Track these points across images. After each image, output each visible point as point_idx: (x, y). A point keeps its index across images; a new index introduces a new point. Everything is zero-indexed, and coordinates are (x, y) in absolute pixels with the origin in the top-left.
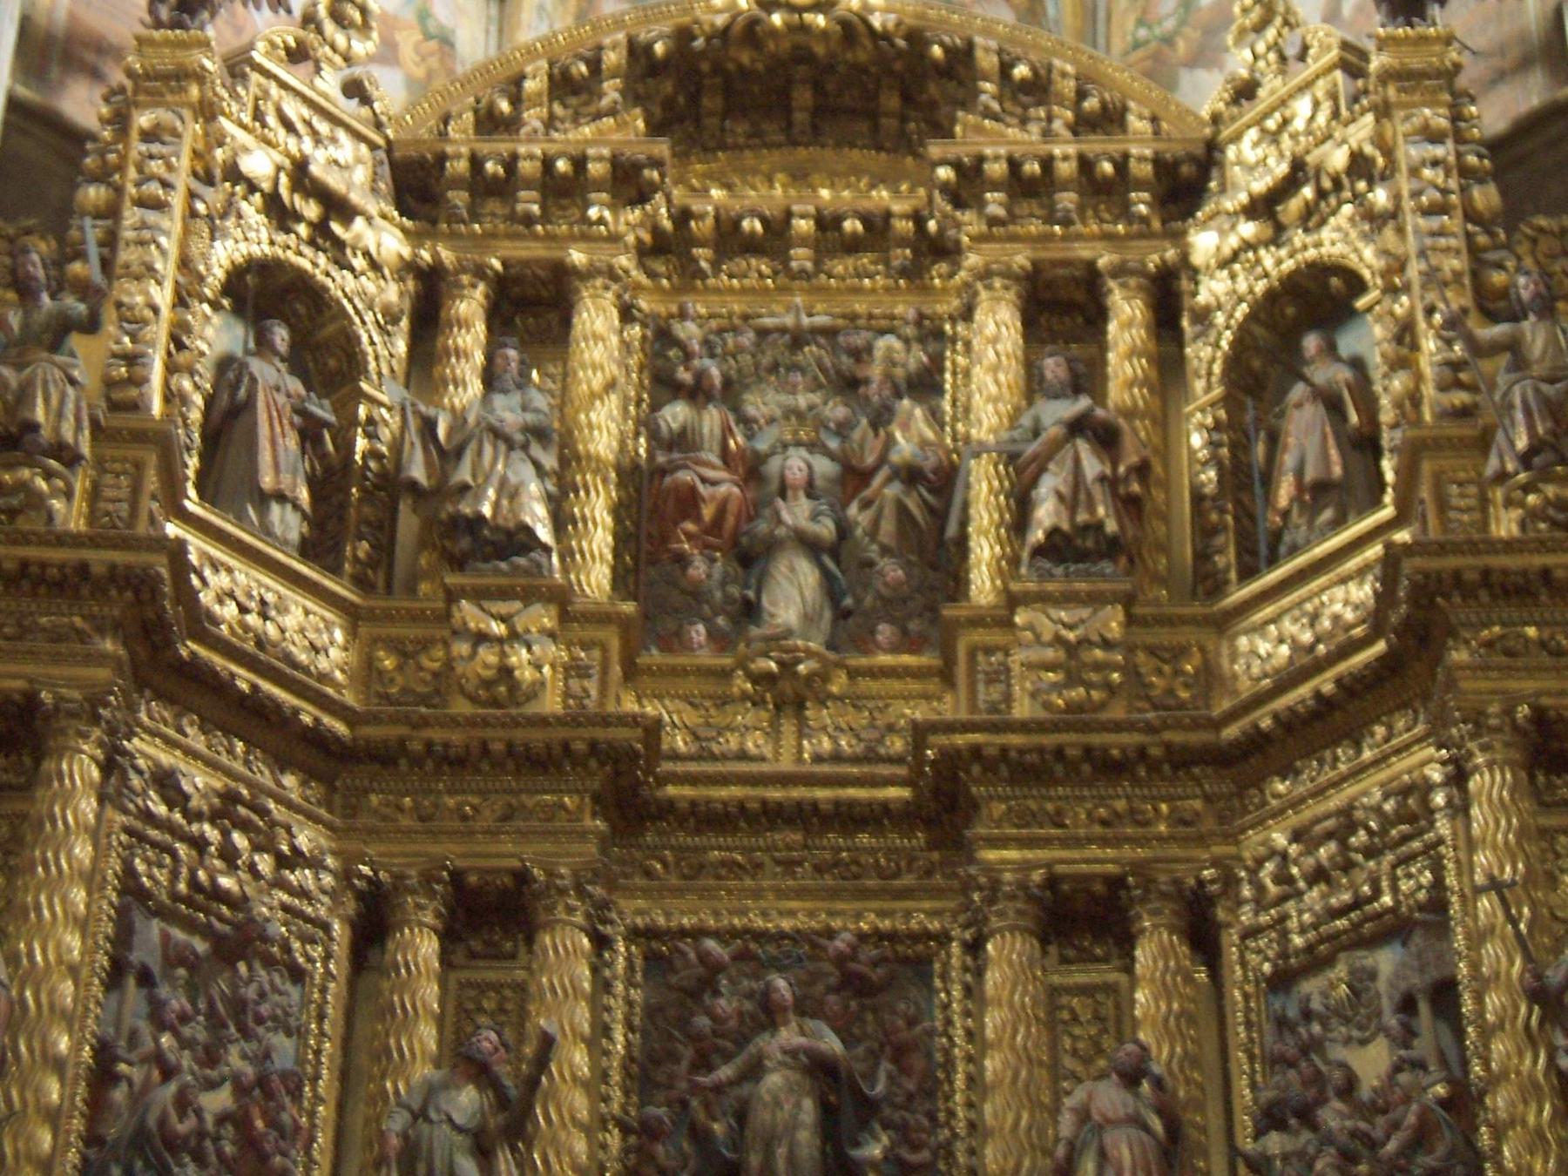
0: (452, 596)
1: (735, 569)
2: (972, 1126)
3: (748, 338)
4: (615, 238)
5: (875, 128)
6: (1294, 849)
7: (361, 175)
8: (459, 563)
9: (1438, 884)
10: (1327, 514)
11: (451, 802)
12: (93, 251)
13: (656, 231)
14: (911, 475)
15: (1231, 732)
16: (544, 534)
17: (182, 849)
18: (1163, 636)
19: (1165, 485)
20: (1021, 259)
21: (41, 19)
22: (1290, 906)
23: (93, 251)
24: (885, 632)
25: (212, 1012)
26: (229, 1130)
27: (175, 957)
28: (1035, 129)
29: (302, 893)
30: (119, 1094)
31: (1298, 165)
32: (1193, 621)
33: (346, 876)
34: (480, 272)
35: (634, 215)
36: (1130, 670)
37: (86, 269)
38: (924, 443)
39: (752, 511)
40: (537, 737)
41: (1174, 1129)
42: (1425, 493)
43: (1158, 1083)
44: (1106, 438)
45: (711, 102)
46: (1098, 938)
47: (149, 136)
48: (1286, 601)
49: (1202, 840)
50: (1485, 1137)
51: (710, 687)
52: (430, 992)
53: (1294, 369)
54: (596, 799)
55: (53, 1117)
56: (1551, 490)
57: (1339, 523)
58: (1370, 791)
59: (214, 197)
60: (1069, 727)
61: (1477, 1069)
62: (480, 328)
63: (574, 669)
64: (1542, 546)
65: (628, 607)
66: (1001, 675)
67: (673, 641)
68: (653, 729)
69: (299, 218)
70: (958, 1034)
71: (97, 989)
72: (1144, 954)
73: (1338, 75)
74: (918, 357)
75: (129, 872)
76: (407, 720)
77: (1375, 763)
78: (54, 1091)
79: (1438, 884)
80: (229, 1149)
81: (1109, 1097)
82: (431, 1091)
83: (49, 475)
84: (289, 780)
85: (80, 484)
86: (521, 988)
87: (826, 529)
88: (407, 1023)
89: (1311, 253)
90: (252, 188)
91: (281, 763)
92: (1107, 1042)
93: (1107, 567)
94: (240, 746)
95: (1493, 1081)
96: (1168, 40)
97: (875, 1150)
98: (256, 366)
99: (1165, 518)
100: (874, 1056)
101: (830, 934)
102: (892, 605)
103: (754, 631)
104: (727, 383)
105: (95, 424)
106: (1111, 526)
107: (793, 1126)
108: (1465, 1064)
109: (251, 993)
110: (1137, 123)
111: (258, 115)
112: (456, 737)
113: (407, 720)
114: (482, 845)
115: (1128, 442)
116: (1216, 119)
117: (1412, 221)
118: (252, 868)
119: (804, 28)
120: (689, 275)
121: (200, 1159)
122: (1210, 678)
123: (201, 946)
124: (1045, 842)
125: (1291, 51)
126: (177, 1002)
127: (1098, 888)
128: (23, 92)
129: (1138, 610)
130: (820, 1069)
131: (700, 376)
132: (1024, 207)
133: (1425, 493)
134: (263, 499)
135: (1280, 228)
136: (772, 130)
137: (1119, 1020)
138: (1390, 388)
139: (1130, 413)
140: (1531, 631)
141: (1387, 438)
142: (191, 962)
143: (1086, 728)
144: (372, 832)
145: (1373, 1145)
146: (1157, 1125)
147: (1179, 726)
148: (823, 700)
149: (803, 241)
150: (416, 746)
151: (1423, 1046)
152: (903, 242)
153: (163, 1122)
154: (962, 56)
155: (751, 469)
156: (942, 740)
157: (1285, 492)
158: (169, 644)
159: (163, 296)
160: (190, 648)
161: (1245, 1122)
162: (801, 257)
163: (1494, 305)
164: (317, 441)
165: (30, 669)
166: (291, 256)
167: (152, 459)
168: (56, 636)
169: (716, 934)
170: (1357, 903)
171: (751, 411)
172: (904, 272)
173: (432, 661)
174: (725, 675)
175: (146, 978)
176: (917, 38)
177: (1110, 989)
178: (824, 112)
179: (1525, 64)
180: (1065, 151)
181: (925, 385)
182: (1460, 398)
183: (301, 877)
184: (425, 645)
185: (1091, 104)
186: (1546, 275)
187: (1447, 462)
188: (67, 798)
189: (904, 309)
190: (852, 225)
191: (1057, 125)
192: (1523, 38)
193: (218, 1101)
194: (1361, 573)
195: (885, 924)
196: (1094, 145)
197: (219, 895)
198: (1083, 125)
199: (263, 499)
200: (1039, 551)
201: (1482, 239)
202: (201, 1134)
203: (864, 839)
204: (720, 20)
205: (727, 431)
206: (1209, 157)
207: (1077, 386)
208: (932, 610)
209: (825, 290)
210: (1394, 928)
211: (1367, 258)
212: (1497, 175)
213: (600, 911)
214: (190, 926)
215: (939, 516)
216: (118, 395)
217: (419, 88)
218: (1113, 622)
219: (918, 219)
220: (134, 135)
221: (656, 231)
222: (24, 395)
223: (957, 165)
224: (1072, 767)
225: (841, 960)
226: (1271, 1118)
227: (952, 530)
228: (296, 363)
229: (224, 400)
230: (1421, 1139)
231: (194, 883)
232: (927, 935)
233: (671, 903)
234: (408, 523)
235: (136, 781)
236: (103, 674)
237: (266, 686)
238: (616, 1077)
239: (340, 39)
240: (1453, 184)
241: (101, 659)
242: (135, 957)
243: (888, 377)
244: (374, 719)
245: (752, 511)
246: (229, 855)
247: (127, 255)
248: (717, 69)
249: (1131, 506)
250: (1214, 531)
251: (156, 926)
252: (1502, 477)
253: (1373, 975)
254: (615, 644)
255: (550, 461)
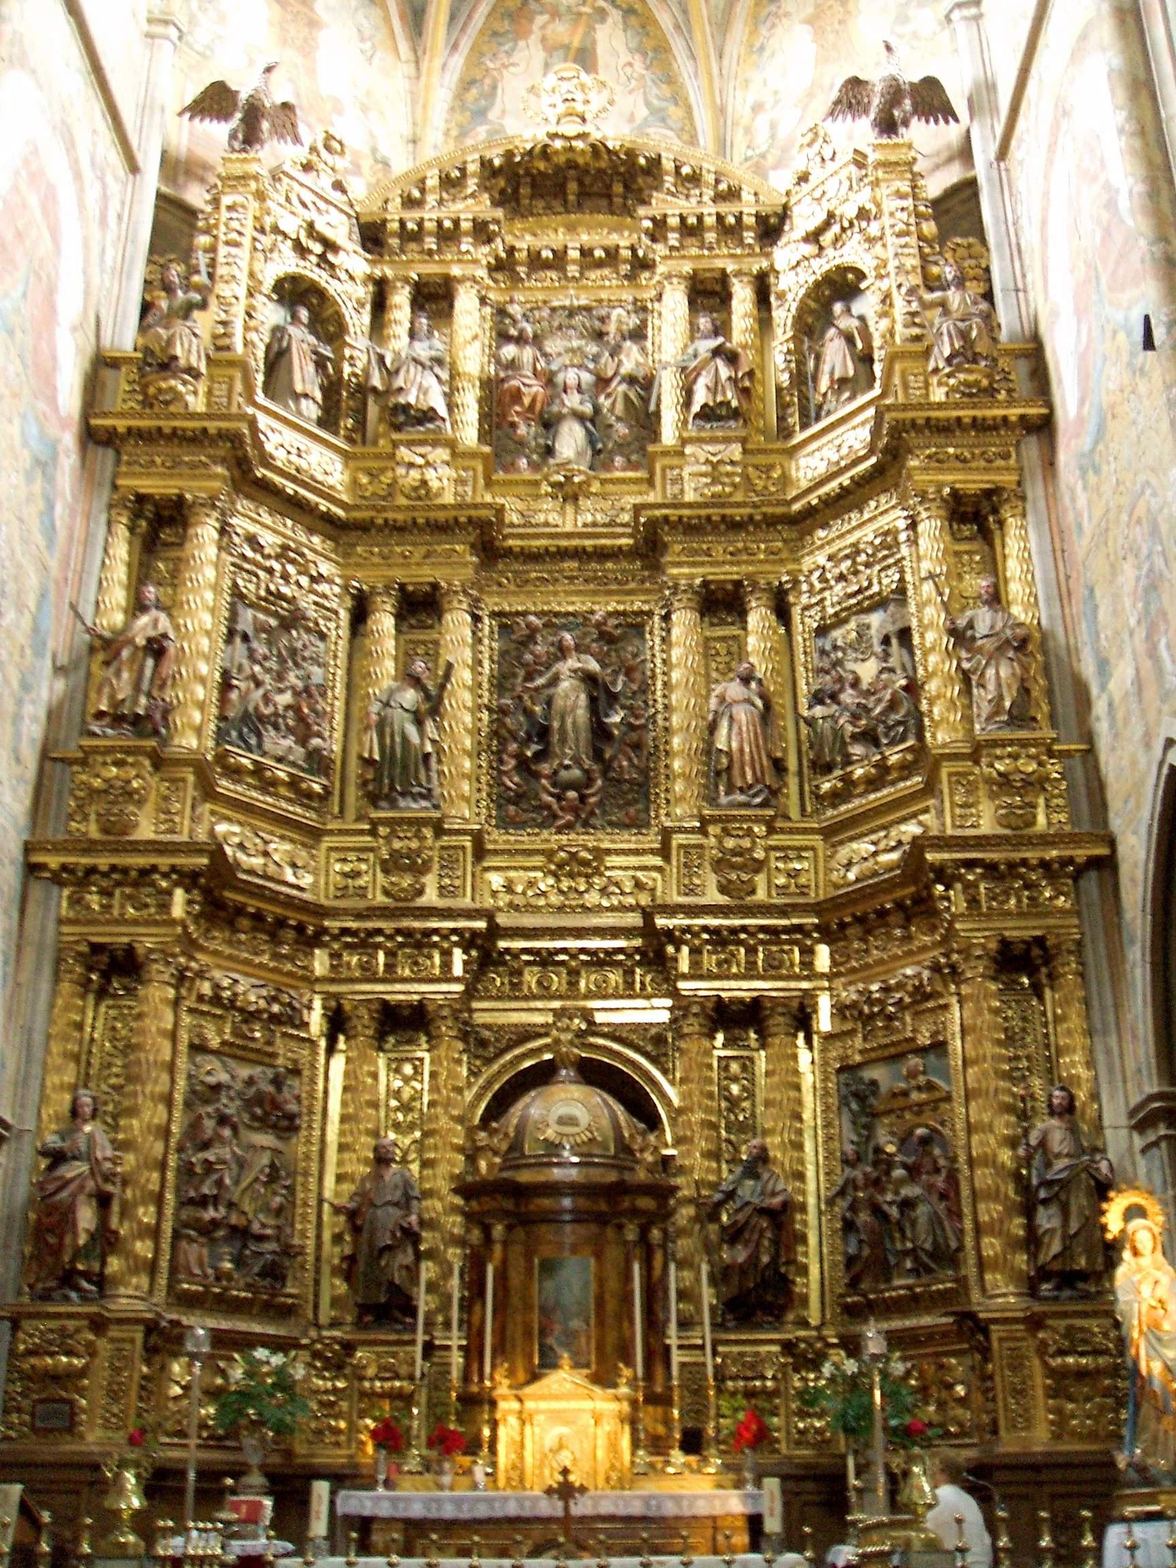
0: (395, 445)
1: (541, 430)
2: (666, 707)
3: (546, 313)
4: (475, 262)
5: (611, 203)
6: (829, 565)
7: (345, 230)
8: (398, 428)
9: (902, 580)
10: (847, 395)
11: (398, 549)
12: (203, 269)
13: (497, 258)
14: (631, 380)
15: (796, 507)
16: (442, 411)
17: (261, 574)
18: (761, 459)
19: (763, 384)
20: (687, 268)
21: (173, 152)
22: (827, 594)
23: (203, 269)
24: (619, 460)
25: (280, 655)
26: (290, 713)
27: (261, 628)
28: (694, 201)
29: (325, 596)
30: (234, 695)
31: (831, 215)
32: (778, 451)
33: (346, 588)
34: (406, 280)
35: (486, 249)
36: (746, 477)
37: (200, 279)
38: (638, 364)
39: (550, 401)
40: (441, 516)
41: (768, 706)
42: (897, 380)
43: (760, 682)
44: (732, 358)
45: (525, 191)
46: (729, 613)
47: (230, 208)
48: (824, 440)
49: (782, 561)
50: (924, 706)
51: (530, 490)
52: (390, 645)
53: (827, 319)
54: (473, 546)
55: (201, 706)
56: (962, 376)
57: (852, 398)
58: (867, 534)
59: (267, 241)
60: (714, 505)
61: (921, 671)
62: (407, 309)
63: (460, 481)
64: (957, 406)
65: (487, 449)
66: (679, 480)
67: (510, 467)
68: (500, 510)
69: (310, 252)
70: (658, 661)
71: (221, 645)
72: (753, 619)
73: (853, 168)
74: (634, 321)
75: (235, 585)
76: (374, 507)
77: (870, 520)
78: (200, 693)
79: (902, 580)
80: (291, 723)
81: (735, 690)
82: (392, 692)
83: (185, 383)
84: (316, 540)
85: (202, 388)
86: (436, 643)
87: (588, 409)
88: (380, 658)
89: (838, 262)
90: (285, 236)
91: (311, 531)
92: (734, 664)
93: (732, 423)
94: (289, 523)
95: (930, 676)
96: (763, 156)
97: (616, 719)
98: (292, 330)
99: (763, 400)
100: (616, 673)
101: (592, 612)
102: (621, 447)
103: (551, 461)
104: (536, 336)
105: (208, 357)
106: (734, 403)
107: (575, 707)
108: (915, 669)
109: (299, 645)
110: (747, 196)
111: (288, 199)
112: (400, 517)
113: (374, 507)
114: (414, 570)
115: (743, 359)
116: (788, 194)
117: (890, 240)
118: (298, 584)
119: (571, 149)
120: (516, 279)
121: (276, 727)
122: (785, 480)
123: (273, 622)
124: (702, 564)
125: (827, 156)
126: (262, 649)
127: (729, 587)
128: (165, 189)
129: (749, 446)
130: (589, 679)
131: (522, 331)
132: (689, 241)
133: (897, 380)
134: (297, 397)
135: (821, 248)
136: (557, 205)
137: (740, 653)
138: (878, 328)
139: (745, 347)
140: (951, 450)
141: (877, 355)
142: (268, 630)
143: (723, 505)
144: (358, 565)
145: (868, 711)
146: (759, 703)
147: (770, 504)
148: (588, 496)
149: (574, 262)
150: (380, 521)
151: (893, 662)
152: (625, 261)
153: (256, 708)
154: (656, 162)
155: (549, 380)
156: (649, 513)
157: (824, 384)
158: (251, 470)
159: (242, 292)
160: (261, 472)
161: (803, 702)
162: (573, 270)
163: (932, 283)
164: (324, 367)
165: (180, 483)
166: (307, 273)
167: (238, 375)
168: (193, 466)
169: (536, 614)
170: (859, 591)
171: (548, 350)
172: (626, 277)
173: (386, 479)
174: (536, 484)
175: (245, 638)
176: (631, 154)
177: (734, 637)
178: (584, 194)
179: (950, 160)
180: (710, 211)
181: (638, 335)
182: (916, 331)
183: (323, 588)
184: (383, 470)
185: (723, 187)
186: (961, 269)
187: (908, 364)
188: (201, 547)
189: (627, 296)
190: (598, 253)
191: (706, 198)
192: (949, 147)
193: (285, 699)
194: (863, 423)
195: (621, 608)
196: (724, 208)
197: (281, 596)
198: (719, 197)
199: (297, 397)
200: (697, 416)
201: (927, 250)
202: (276, 714)
203: (609, 565)
204: (528, 146)
205: (536, 359)
206: (784, 214)
207: (716, 333)
208: (643, 449)
209: (586, 288)
210: (880, 603)
211: (866, 263)
212: (936, 218)
213: (476, 602)
214: (267, 612)
215: (645, 401)
216: (221, 342)
217: (372, 188)
218: (735, 451)
219: (633, 249)
220: (223, 209)
221: (497, 258)
222: (170, 342)
223: (653, 219)
224: (715, 527)
225: (598, 625)
226: (818, 698)
227: (652, 408)
228: (313, 327)
229: (275, 347)
230: (893, 705)
231: (268, 590)
232: (641, 613)
233: (512, 599)
234: (373, 410)
235: (236, 540)
236: (216, 484)
237: (302, 492)
238: (486, 685)
239: (330, 162)
240: (912, 220)
241: (216, 477)
242: (240, 627)
243: (619, 330)
244: (357, 507)
245: (550, 401)
246: (285, 577)
247: (221, 271)
248: (528, 173)
249: (745, 392)
250: (788, 405)
251: (250, 613)
252: (936, 370)
253: (868, 627)
254: (480, 468)
255: (445, 376)
